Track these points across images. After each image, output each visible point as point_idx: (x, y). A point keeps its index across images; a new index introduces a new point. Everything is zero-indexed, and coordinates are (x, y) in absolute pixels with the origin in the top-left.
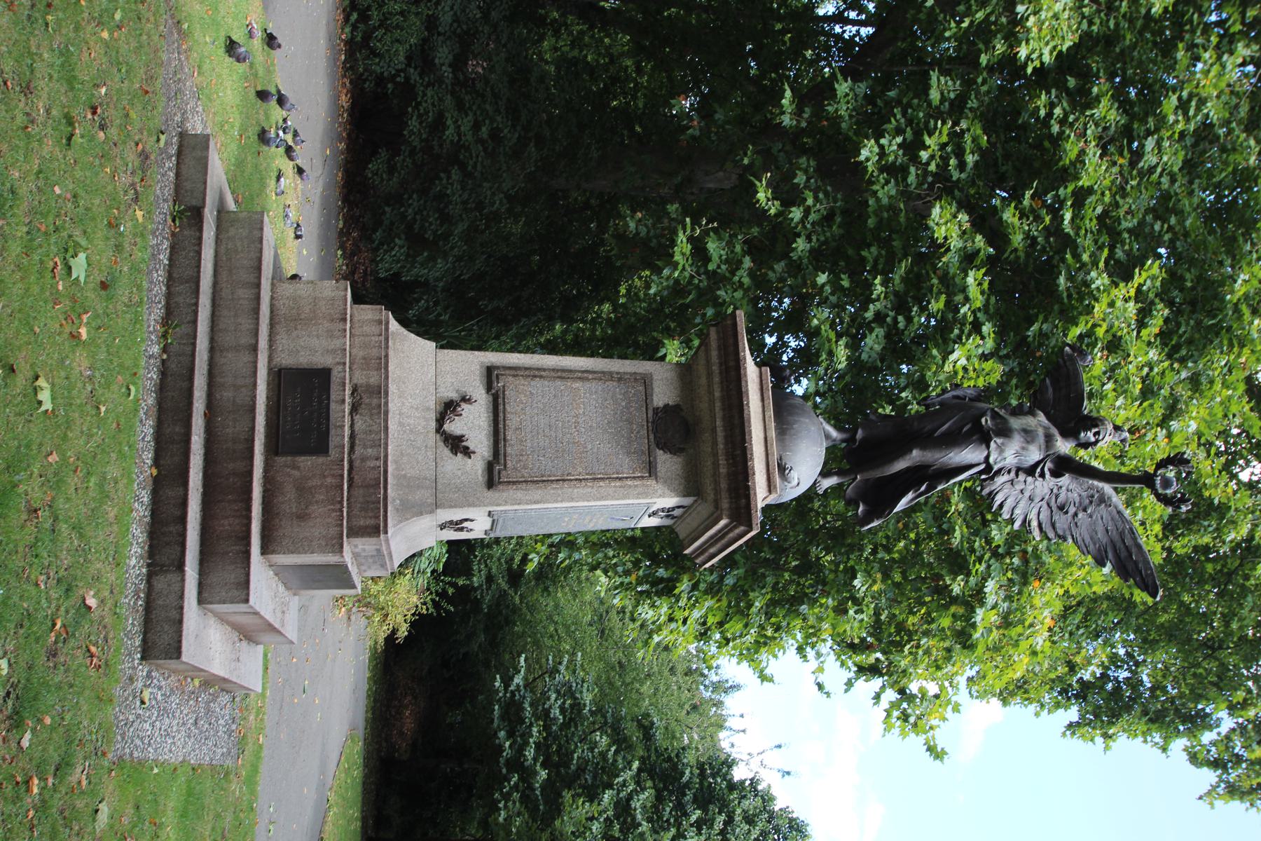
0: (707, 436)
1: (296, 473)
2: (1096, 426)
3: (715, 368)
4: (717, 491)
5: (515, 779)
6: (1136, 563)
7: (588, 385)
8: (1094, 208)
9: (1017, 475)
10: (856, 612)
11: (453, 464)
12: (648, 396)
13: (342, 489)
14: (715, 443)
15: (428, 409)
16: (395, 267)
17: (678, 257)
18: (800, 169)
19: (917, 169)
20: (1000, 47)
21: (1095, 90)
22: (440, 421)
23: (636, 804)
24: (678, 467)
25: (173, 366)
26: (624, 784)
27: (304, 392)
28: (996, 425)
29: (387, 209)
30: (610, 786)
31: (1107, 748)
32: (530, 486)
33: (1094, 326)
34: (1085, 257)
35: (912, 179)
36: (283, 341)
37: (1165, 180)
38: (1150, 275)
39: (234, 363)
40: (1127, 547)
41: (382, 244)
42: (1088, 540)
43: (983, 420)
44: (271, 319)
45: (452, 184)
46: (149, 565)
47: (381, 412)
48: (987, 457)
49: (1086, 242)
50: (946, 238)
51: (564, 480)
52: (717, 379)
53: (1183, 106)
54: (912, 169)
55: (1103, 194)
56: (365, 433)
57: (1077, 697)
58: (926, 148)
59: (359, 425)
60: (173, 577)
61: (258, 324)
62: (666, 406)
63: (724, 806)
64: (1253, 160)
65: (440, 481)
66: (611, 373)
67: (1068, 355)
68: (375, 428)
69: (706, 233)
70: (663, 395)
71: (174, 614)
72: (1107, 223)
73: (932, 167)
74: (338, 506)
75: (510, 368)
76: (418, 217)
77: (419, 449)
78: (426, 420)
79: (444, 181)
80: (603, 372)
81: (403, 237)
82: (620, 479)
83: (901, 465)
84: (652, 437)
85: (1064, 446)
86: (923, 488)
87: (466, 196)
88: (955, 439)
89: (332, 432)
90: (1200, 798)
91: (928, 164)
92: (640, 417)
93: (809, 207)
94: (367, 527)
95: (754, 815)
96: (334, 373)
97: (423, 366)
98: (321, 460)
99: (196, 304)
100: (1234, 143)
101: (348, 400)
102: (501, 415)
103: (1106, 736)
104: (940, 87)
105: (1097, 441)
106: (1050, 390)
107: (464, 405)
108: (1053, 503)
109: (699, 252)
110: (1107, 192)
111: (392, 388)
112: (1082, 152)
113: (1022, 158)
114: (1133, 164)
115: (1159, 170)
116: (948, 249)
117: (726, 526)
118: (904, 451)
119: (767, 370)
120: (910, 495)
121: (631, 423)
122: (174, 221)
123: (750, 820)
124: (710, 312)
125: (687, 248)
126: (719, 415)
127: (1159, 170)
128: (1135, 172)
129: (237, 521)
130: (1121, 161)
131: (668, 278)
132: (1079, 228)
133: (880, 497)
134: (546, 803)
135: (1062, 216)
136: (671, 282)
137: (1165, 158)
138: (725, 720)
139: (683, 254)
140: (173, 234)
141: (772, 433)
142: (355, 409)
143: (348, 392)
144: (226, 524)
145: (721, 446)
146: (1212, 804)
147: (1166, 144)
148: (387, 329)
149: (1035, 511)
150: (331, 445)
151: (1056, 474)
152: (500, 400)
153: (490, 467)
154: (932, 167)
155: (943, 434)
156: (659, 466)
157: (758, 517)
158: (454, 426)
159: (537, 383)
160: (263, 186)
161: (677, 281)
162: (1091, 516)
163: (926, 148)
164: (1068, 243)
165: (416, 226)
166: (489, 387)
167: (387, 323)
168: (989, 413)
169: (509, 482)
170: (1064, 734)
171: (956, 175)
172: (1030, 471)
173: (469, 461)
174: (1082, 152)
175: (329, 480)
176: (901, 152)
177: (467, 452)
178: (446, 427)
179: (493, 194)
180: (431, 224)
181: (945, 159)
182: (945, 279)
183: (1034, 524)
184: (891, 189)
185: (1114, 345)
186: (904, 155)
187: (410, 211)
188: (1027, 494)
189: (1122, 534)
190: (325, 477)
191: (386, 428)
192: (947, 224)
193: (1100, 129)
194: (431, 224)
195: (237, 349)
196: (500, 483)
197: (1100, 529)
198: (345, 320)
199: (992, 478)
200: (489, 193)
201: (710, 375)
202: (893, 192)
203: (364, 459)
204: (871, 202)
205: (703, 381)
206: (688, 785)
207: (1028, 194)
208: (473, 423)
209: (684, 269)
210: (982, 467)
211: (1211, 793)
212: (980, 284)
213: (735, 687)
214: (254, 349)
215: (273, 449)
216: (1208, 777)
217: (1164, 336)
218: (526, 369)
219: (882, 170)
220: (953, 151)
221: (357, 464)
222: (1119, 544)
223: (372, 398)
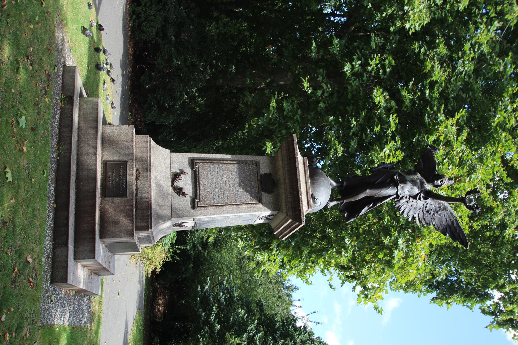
0: (282, 186)
9: (409, 199)
12: (258, 170)
13: (133, 211)
15: (168, 177)
17: (271, 108)
19: (367, 74)
20: (398, 24)
21: (437, 41)
22: (173, 181)
23: (257, 338)
26: (251, 330)
29: (149, 95)
35: (365, 78)
38: (462, 114)
43: (395, 177)
46: (53, 244)
50: (379, 102)
53: (473, 46)
54: (365, 75)
55: (442, 83)
57: (436, 288)
58: (370, 65)
62: (266, 174)
66: (242, 161)
68: (146, 185)
73: (373, 74)
74: (131, 218)
82: (247, 204)
83: (362, 196)
84: (260, 187)
85: (428, 187)
86: (371, 205)
90: (486, 327)
94: (143, 226)
98: (124, 199)
101: (135, 174)
104: (375, 41)
106: (422, 164)
107: (182, 175)
109: (280, 109)
112: (433, 67)
113: (409, 68)
114: (453, 71)
115: (464, 73)
116: (380, 107)
117: (291, 222)
118: (363, 190)
120: (366, 208)
121: (251, 181)
122: (61, 102)
127: (464, 73)
133: (354, 209)
138: (292, 302)
140: (61, 108)
141: (309, 184)
146: (491, 330)
148: (150, 145)
149: (417, 214)
151: (425, 198)
152: (197, 173)
156: (263, 199)
157: (304, 219)
158: (177, 184)
163: (370, 65)
166: (192, 167)
174: (433, 67)
178: (175, 184)
183: (417, 219)
187: (159, 96)
188: (414, 207)
191: (151, 185)
192: (379, 97)
196: (198, 207)
197: (444, 220)
199: (399, 201)
202: (358, 84)
204: (349, 87)
207: (411, 84)
208: (186, 183)
209: (273, 114)
210: (395, 196)
213: (297, 288)
216: (490, 319)
221: (139, 200)
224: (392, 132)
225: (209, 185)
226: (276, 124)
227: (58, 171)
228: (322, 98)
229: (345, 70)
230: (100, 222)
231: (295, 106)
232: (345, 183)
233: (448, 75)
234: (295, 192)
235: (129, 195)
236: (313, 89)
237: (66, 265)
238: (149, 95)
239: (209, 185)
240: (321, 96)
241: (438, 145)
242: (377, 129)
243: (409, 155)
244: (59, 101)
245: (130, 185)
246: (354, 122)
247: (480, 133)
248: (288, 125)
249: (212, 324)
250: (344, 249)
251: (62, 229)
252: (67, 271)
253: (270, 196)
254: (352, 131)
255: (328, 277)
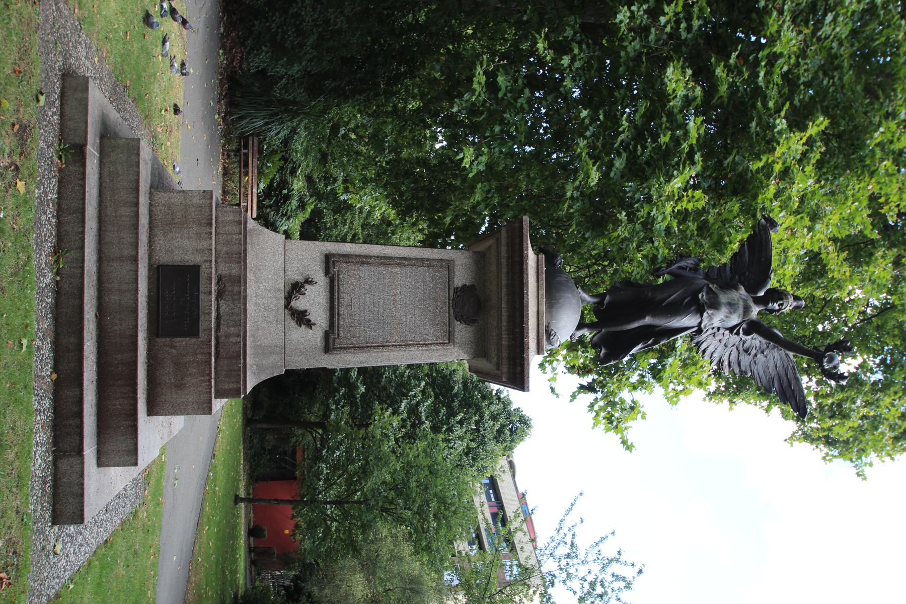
1: (174, 351)
2: (781, 299)
3: (504, 261)
4: (499, 357)
5: (343, 391)
6: (793, 391)
7: (404, 270)
8: (783, 66)
10: (583, 352)
11: (298, 333)
12: (450, 279)
13: (210, 365)
14: (500, 319)
15: (279, 290)
16: (262, 66)
17: (475, 86)
18: (569, 26)
19: (657, 30)
22: (289, 298)
23: (422, 409)
24: (466, 261)
25: (65, 286)
26: (415, 396)
27: (177, 287)
28: (709, 299)
29: (256, 22)
30: (406, 395)
31: (731, 409)
32: (357, 350)
33: (774, 162)
34: (771, 104)
35: (652, 37)
36: (161, 242)
37: (835, 45)
38: (819, 125)
39: (117, 270)
40: (788, 379)
41: (252, 49)
42: (761, 373)
43: (700, 296)
44: (150, 223)
45: (306, 8)
46: (53, 452)
47: (241, 298)
48: (700, 323)
49: (773, 93)
50: (674, 91)
51: (383, 346)
52: (504, 270)
54: (653, 30)
55: (790, 57)
56: (228, 315)
59: (224, 308)
60: (74, 461)
61: (137, 238)
62: (464, 286)
63: (479, 410)
64: (901, 36)
65: (288, 346)
66: (422, 260)
67: (763, 226)
68: (236, 310)
69: (497, 69)
70: (461, 278)
71: (76, 489)
72: (790, 79)
73: (668, 29)
74: (207, 378)
75: (344, 256)
76: (280, 30)
77: (271, 322)
78: (277, 299)
79: (300, 5)
80: (416, 259)
81: (268, 44)
82: (426, 345)
84: (452, 312)
86: (650, 342)
87: (316, 16)
88: (677, 309)
89: (202, 318)
90: (786, 440)
91: (665, 26)
92: (444, 296)
93: (575, 55)
94: (230, 390)
95: (498, 414)
96: (203, 269)
97: (274, 255)
98: (193, 340)
99: (83, 233)
100: (889, 21)
101: (214, 288)
102: (336, 294)
103: (731, 402)
105: (780, 309)
107: (307, 286)
108: (741, 348)
109: (492, 86)
110: (793, 56)
111: (250, 276)
115: (832, 37)
119: (542, 257)
120: (640, 346)
121: (436, 301)
122: (60, 158)
123: (494, 417)
124: (497, 129)
125: (483, 79)
126: (504, 299)
127: (832, 37)
128: (814, 40)
129: (126, 402)
130: (806, 31)
131: (467, 101)
132: (769, 82)
134: (362, 407)
135: (759, 72)
136: (469, 103)
137: (838, 29)
139: (479, 83)
140: (60, 170)
141: (543, 308)
142: (220, 295)
143: (214, 281)
144: (117, 404)
145: (505, 324)
146: (792, 444)
147: (841, 19)
148: (245, 228)
149: (727, 354)
150: (201, 328)
151: (747, 333)
152: (336, 283)
153: (327, 335)
154: (668, 29)
155: (670, 304)
156: (456, 334)
158: (299, 304)
159: (365, 268)
160: (150, 56)
161: (473, 104)
162: (766, 357)
163: (664, 14)
164: (758, 93)
165: (279, 38)
166: (327, 272)
167: (246, 222)
168: (705, 289)
169: (341, 348)
170: (704, 399)
171: (684, 35)
172: (731, 330)
173: (311, 331)
175: (200, 357)
176: (645, 16)
177: (309, 324)
178: (293, 304)
179: (337, 17)
180: (289, 36)
181: (678, 22)
182: (670, 115)
183: (726, 363)
184: (636, 44)
185: (786, 173)
186: (648, 18)
187: (274, 25)
188: (723, 343)
189: (786, 370)
190: (196, 354)
191: (245, 310)
192: (677, 80)
193: (794, 4)
194: (289, 36)
195: (121, 259)
196: (334, 348)
197: (771, 365)
198: (210, 224)
200: (333, 16)
201: (499, 265)
202: (638, 47)
203: (228, 336)
204: (623, 54)
205: (494, 268)
206: (456, 395)
208: (314, 301)
209: (479, 95)
210: (695, 329)
211: (792, 437)
212: (698, 129)
214: (135, 259)
215: (154, 332)
217: (820, 165)
218: (357, 256)
219: (630, 30)
220: (684, 17)
221: (222, 339)
222: (784, 378)
223: (233, 287)
224: (691, 146)
225: (357, 306)
226: (482, 114)
227: (57, 307)
228: (571, 70)
229: (617, 21)
230: (148, 385)
231: (520, 81)
232: (607, 298)
233: (805, 41)
234: (517, 330)
235: (203, 335)
236: (554, 53)
237: (79, 491)
238: (256, 22)
239: (357, 306)
240: (570, 66)
241: (768, 177)
242: (664, 139)
243: (713, 186)
244: (56, 159)
245: (205, 314)
246: (624, 122)
247: (844, 152)
248: (505, 119)
249: (354, 383)
250: (582, 347)
251: (71, 422)
252: (83, 503)
253: (469, 328)
254: (620, 139)
255: (550, 375)
